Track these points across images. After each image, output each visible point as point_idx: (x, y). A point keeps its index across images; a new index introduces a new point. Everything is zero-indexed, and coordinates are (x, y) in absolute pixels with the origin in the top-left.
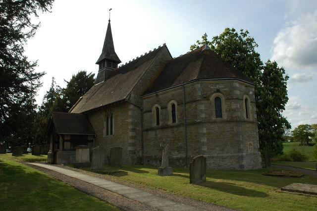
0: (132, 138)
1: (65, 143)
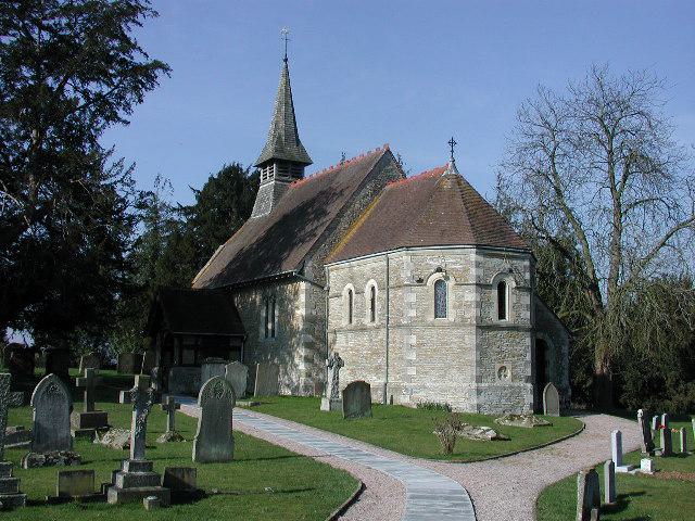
1: (185, 351)
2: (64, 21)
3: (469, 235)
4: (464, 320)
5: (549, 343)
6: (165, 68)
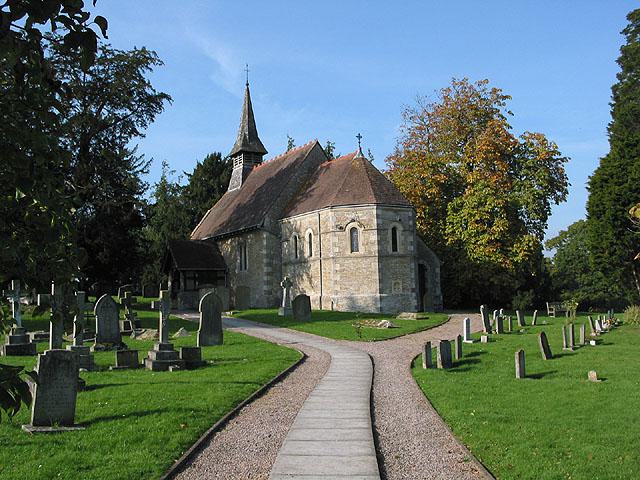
0: (268, 274)
2: (101, 68)
3: (372, 197)
4: (370, 252)
5: (425, 263)
6: (169, 98)
